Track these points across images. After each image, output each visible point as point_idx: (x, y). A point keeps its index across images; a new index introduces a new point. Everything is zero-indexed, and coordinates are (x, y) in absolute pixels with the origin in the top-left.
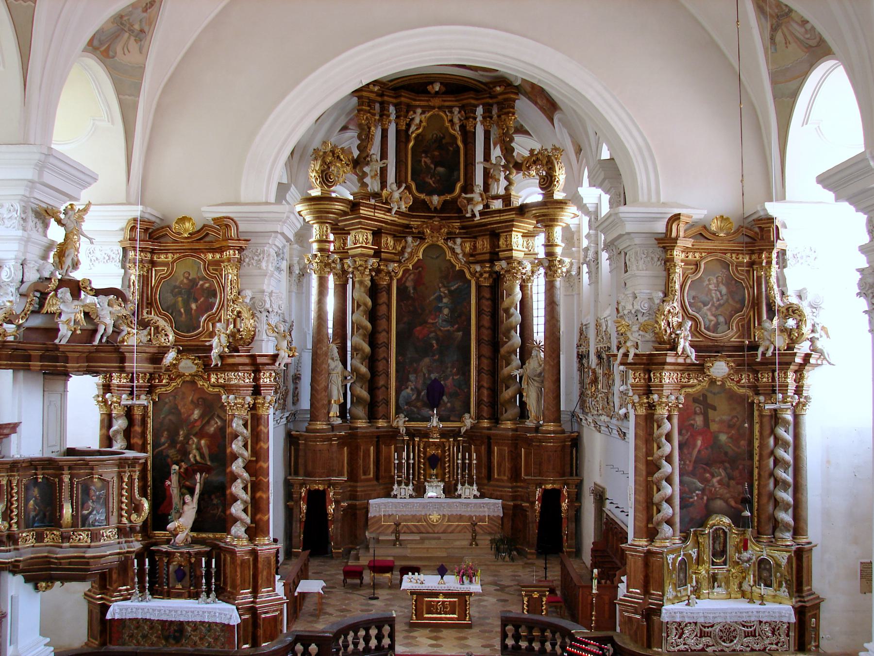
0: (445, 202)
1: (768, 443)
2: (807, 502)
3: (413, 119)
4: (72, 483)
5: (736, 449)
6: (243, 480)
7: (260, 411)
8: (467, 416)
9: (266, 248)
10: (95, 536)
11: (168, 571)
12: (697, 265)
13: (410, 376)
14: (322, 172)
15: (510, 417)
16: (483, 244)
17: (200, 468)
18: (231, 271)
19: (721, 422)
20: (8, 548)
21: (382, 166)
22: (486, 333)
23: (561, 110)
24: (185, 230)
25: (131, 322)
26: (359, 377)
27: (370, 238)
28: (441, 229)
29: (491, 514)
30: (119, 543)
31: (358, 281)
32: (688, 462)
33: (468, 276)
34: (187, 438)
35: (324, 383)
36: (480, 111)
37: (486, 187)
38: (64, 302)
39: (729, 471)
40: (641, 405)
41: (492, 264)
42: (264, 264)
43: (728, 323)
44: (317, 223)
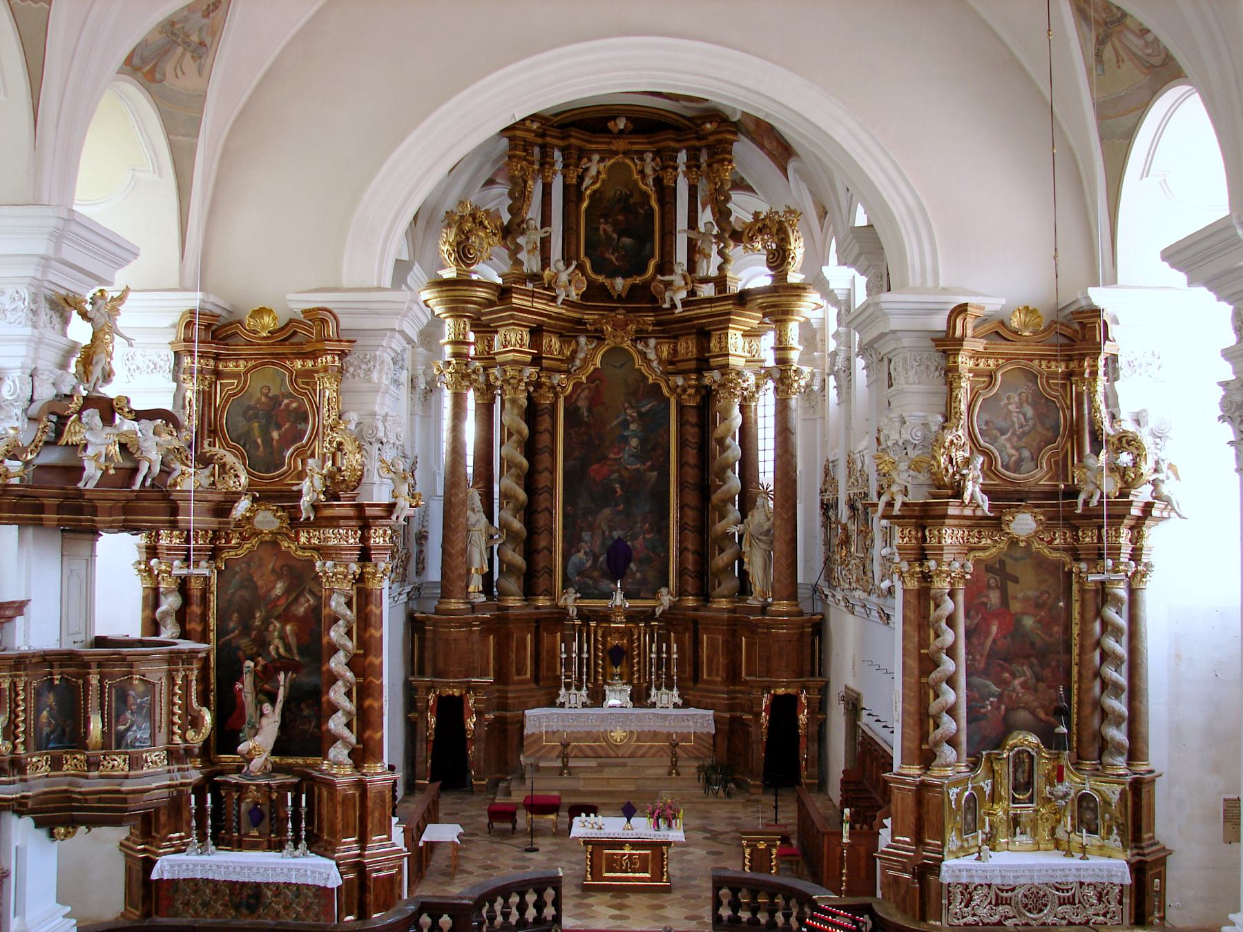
0: (633, 286)
1: (1092, 629)
2: (1147, 713)
3: (587, 169)
4: (102, 687)
5: (1046, 638)
6: (346, 681)
7: (370, 584)
8: (664, 590)
9: (378, 353)
10: (135, 762)
11: (239, 811)
12: (991, 376)
13: (583, 534)
14: (458, 244)
15: (726, 592)
16: (687, 347)
17: (285, 664)
18: (328, 385)
19: (1026, 599)
20: (12, 778)
21: (543, 236)
22: (691, 473)
23: (798, 156)
24: (264, 327)
25: (187, 457)
26: (511, 535)
27: (527, 337)
28: (627, 325)
29: (699, 731)
30: (169, 771)
31: (510, 400)
32: (978, 657)
33: (665, 392)
34: (266, 622)
35: (461, 544)
36: (682, 157)
37: (692, 266)
38: (91, 429)
39: (1037, 669)
40: (912, 575)
41: (700, 376)
42: (375, 376)
43: (1035, 459)
44: (451, 316)
